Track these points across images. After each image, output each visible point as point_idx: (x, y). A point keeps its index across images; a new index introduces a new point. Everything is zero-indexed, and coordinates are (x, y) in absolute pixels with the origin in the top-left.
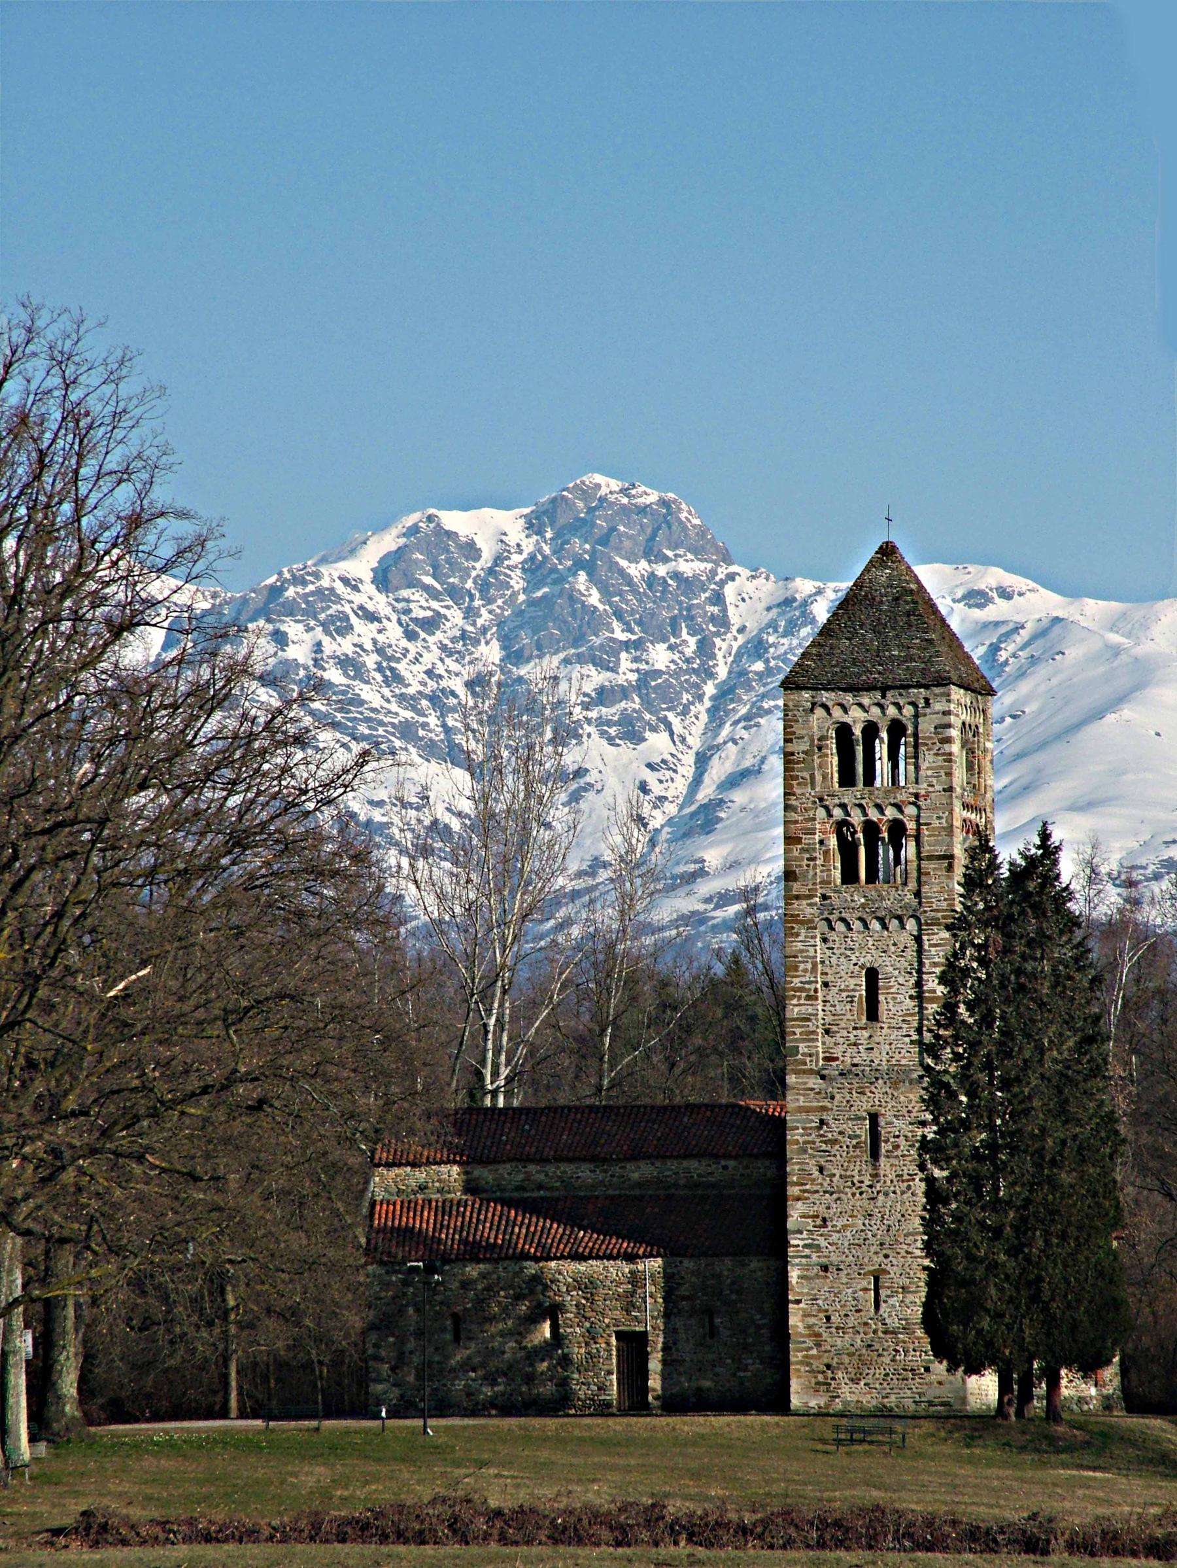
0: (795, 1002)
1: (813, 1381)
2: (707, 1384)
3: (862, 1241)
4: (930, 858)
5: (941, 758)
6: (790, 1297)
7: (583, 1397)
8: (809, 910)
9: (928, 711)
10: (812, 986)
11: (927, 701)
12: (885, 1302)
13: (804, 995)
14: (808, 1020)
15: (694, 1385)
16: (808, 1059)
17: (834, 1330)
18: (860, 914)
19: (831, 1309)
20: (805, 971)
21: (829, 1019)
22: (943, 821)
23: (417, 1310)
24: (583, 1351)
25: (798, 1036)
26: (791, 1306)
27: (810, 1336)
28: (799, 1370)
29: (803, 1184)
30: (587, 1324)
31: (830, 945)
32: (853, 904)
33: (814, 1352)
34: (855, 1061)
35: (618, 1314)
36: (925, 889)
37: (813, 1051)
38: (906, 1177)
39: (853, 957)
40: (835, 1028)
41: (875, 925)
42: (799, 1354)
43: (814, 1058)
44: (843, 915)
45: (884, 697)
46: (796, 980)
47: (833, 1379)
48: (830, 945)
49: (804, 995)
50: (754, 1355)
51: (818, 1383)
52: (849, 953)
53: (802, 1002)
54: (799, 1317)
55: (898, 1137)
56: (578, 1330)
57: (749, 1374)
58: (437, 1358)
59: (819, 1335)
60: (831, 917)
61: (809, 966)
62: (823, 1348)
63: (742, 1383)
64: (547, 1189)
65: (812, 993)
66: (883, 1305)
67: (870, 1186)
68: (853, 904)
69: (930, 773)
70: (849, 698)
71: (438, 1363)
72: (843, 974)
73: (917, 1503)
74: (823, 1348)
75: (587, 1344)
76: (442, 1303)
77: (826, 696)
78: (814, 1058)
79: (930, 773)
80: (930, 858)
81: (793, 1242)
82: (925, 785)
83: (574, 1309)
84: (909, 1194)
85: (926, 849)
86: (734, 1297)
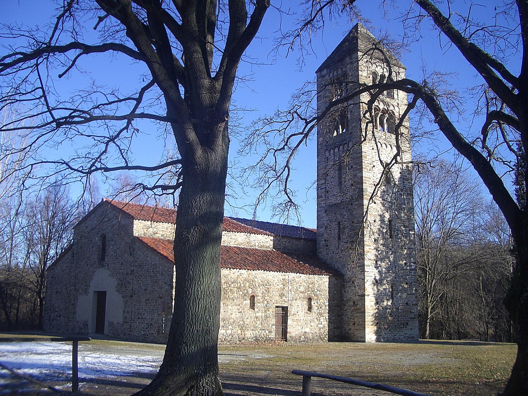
0: (366, 170)
2: (308, 330)
14: (370, 178)
15: (303, 330)
20: (369, 159)
24: (263, 314)
46: (366, 162)
75: (265, 311)
86: (318, 292)
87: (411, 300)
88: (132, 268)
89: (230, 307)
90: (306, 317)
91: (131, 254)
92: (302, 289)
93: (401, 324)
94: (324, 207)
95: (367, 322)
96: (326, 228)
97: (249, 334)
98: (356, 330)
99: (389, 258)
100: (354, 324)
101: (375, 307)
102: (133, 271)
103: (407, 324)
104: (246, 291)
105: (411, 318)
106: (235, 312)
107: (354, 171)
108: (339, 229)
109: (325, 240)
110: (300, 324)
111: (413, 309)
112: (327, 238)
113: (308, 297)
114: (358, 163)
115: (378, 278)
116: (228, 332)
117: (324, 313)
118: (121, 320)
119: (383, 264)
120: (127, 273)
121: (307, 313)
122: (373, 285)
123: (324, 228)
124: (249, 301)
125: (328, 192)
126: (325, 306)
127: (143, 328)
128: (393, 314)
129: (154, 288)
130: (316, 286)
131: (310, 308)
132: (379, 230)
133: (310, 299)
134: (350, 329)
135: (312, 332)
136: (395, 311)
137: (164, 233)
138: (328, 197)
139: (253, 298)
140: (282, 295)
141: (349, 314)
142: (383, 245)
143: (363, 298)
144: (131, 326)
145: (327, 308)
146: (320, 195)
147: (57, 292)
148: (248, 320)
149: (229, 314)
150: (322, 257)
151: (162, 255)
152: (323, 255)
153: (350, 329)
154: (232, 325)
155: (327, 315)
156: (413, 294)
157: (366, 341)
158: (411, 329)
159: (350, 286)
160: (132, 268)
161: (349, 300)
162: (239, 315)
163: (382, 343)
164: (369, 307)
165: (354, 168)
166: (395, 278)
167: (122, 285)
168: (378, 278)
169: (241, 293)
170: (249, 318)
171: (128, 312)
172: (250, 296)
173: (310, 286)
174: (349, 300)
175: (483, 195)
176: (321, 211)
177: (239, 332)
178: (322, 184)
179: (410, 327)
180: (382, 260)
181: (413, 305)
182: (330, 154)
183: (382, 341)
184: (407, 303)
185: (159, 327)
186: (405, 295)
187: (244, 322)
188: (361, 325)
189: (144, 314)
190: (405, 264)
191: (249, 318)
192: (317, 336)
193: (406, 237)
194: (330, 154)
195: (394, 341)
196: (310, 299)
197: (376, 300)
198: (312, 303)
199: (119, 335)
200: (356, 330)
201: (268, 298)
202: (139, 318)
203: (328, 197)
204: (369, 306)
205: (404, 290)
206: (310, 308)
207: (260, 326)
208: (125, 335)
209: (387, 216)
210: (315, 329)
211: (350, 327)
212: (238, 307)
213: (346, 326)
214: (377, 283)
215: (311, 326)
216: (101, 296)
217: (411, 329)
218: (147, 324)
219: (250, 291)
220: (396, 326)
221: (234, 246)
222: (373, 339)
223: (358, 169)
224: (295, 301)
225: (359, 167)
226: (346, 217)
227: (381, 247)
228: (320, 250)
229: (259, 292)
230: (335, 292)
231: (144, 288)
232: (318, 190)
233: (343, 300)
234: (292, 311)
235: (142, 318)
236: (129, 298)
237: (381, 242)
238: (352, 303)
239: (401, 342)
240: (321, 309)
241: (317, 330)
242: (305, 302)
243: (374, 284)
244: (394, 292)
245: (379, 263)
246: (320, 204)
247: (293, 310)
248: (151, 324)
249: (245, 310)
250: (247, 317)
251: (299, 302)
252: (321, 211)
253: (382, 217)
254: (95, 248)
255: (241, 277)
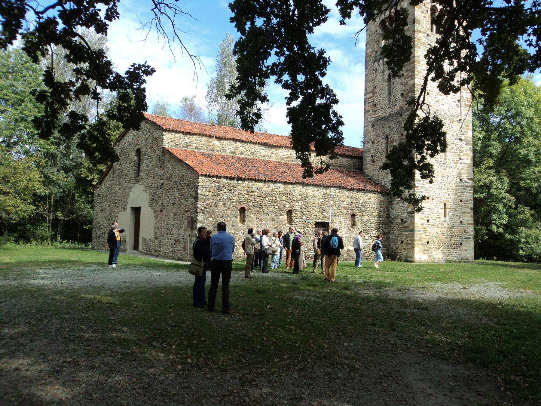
1: (423, 248)
3: (440, 187)
17: (430, 226)
19: (430, 216)
20: (422, 64)
27: (422, 228)
28: (418, 244)
30: (304, 218)
33: (423, 235)
34: (438, 108)
35: (317, 213)
36: (208, 134)
38: (455, 162)
42: (418, 236)
47: (430, 248)
51: (425, 250)
56: (300, 220)
59: (425, 228)
62: (427, 234)
64: (244, 154)
66: (448, 216)
67: (444, 164)
73: (88, 346)
74: (427, 234)
81: (416, 185)
84: (456, 169)
86: (363, 209)
87: (466, 219)
88: (162, 181)
89: (264, 222)
90: (349, 235)
91: (161, 167)
92: (345, 204)
94: (371, 122)
96: (373, 143)
98: (404, 249)
100: (402, 242)
102: (162, 184)
103: (461, 244)
105: (465, 238)
107: (405, 79)
108: (387, 143)
109: (372, 156)
111: (468, 229)
112: (374, 153)
113: (352, 213)
114: (410, 70)
118: (152, 236)
120: (158, 187)
121: (350, 230)
123: (371, 143)
124: (286, 217)
125: (375, 105)
127: (172, 244)
129: (181, 202)
130: (361, 202)
131: (354, 225)
133: (353, 216)
134: (397, 248)
137: (198, 145)
138: (376, 111)
139: (290, 212)
140: (323, 210)
141: (396, 232)
143: (412, 215)
144: (160, 242)
146: (367, 109)
147: (102, 210)
150: (369, 173)
151: (187, 164)
152: (369, 171)
153: (397, 248)
158: (466, 250)
159: (398, 203)
160: (162, 181)
161: (396, 217)
163: (525, 264)
165: (406, 76)
167: (153, 202)
171: (158, 229)
172: (287, 211)
173: (354, 201)
174: (396, 217)
176: (368, 126)
178: (370, 98)
179: (464, 248)
182: (379, 64)
184: (461, 222)
185: (185, 243)
188: (410, 244)
189: (172, 230)
194: (379, 64)
199: (150, 252)
200: (404, 249)
202: (167, 234)
203: (376, 111)
204: (419, 223)
206: (354, 225)
208: (155, 251)
211: (397, 246)
213: (392, 245)
216: (137, 211)
217: (466, 250)
218: (175, 240)
220: (448, 246)
221: (275, 160)
223: (410, 77)
224: (336, 218)
225: (410, 74)
226: (395, 129)
228: (366, 166)
229: (297, 206)
230: (382, 209)
231: (172, 202)
232: (365, 104)
233: (390, 217)
235: (170, 234)
236: (159, 212)
238: (400, 221)
240: (366, 226)
242: (349, 219)
246: (367, 119)
248: (178, 240)
251: (341, 219)
252: (368, 126)
254: (132, 164)
255: (276, 190)
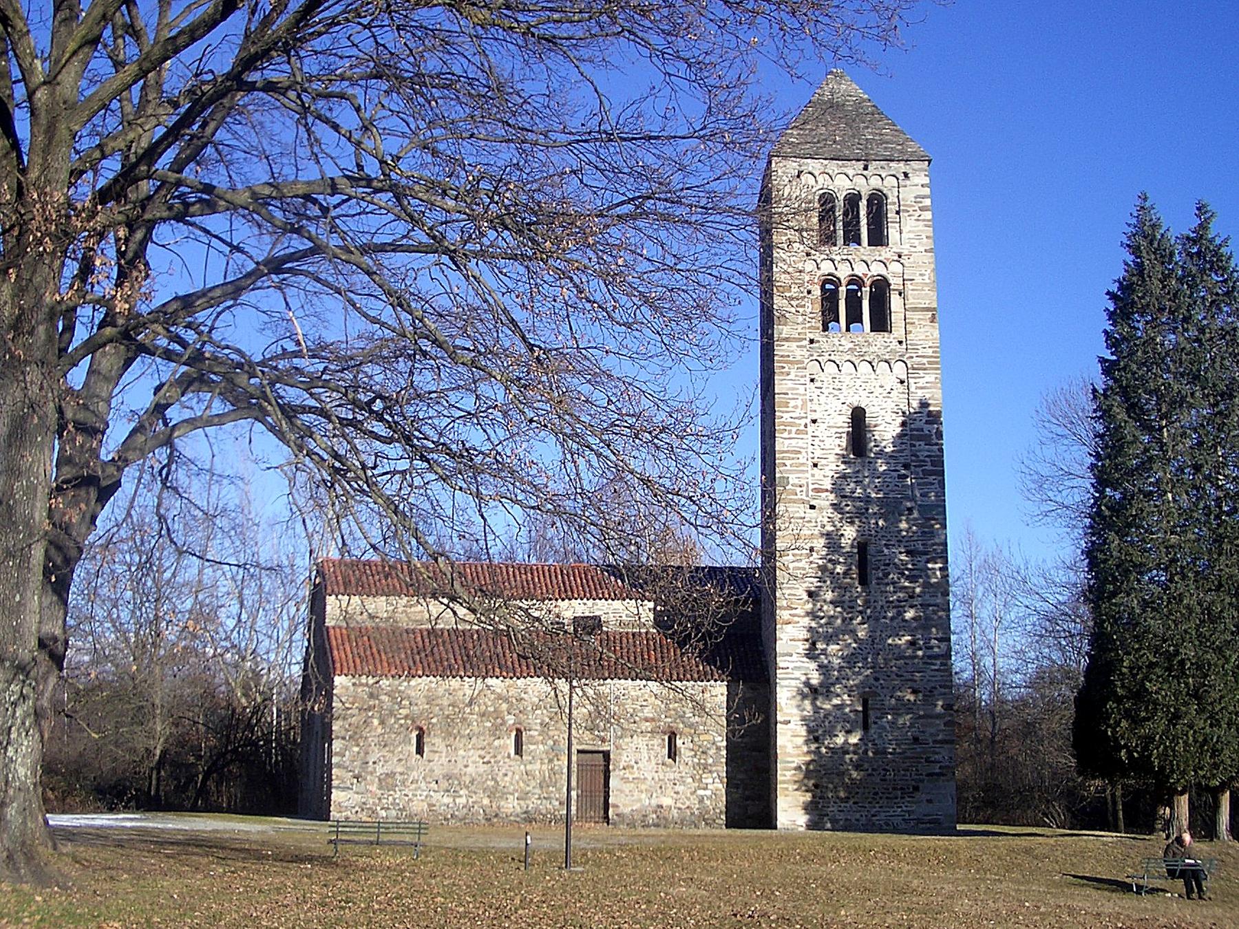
0: (786, 435)
2: (667, 801)
4: (915, 309)
5: (921, 223)
6: (779, 718)
7: (544, 812)
8: (798, 352)
9: (908, 182)
10: (803, 422)
11: (906, 175)
12: (875, 723)
13: (794, 429)
14: (800, 452)
15: (654, 802)
16: (799, 489)
18: (848, 358)
20: (796, 407)
21: (818, 453)
22: (926, 277)
23: (382, 723)
24: (545, 767)
25: (788, 468)
26: (779, 726)
28: (787, 789)
29: (792, 609)
31: (818, 384)
32: (841, 348)
37: (803, 482)
39: (841, 396)
40: (824, 462)
41: (864, 368)
43: (804, 489)
44: (832, 358)
45: (866, 168)
46: (785, 415)
48: (818, 384)
49: (794, 429)
50: (715, 775)
52: (836, 392)
53: (793, 435)
54: (789, 737)
55: (888, 565)
56: (541, 746)
57: (708, 793)
58: (399, 769)
60: (820, 359)
61: (799, 403)
63: (701, 801)
65: (802, 428)
68: (841, 348)
69: (912, 235)
70: (833, 167)
71: (401, 774)
72: (1193, 332)
75: (551, 761)
76: (406, 717)
77: (812, 165)
78: (804, 489)
79: (912, 235)
80: (915, 309)
82: (908, 246)
83: (538, 727)
85: (911, 302)
89: (461, 752)
93: (894, 789)
95: (784, 782)
97: (511, 805)
99: (853, 632)
101: (805, 749)
104: (499, 721)
106: (474, 762)
110: (643, 787)
115: (815, 679)
116: (458, 800)
117: (714, 764)
119: (833, 648)
122: (799, 698)
126: (718, 749)
128: (866, 766)
131: (673, 753)
132: (823, 569)
133: (672, 737)
135: (679, 805)
136: (872, 760)
142: (834, 603)
145: (724, 752)
148: (506, 779)
149: (460, 765)
154: (467, 787)
155: (723, 769)
156: (938, 716)
157: (779, 826)
158: (929, 801)
162: (483, 768)
164: (790, 750)
166: (877, 679)
168: (815, 679)
169: (489, 724)
170: (510, 774)
175: (843, 273)
177: (486, 801)
180: (829, 639)
181: (935, 742)
183: (829, 825)
186: (906, 719)
187: (497, 782)
190: (912, 644)
191: (510, 774)
192: (692, 814)
193: (913, 579)
195: (869, 828)
196: (672, 737)
197: (810, 731)
198: (679, 742)
201: (557, 733)
204: (790, 745)
205: (902, 707)
206: (673, 753)
207: (538, 791)
209: (850, 533)
210: (689, 799)
212: (482, 753)
214: (812, 692)
215: (677, 793)
219: (511, 720)
222: (799, 823)
227: (830, 610)
234: (621, 759)
237: (829, 596)
239: (896, 830)
241: (694, 802)
243: (804, 697)
244: (871, 712)
245: (820, 646)
247: (624, 758)
249: (499, 757)
250: (504, 771)
253: (833, 542)
